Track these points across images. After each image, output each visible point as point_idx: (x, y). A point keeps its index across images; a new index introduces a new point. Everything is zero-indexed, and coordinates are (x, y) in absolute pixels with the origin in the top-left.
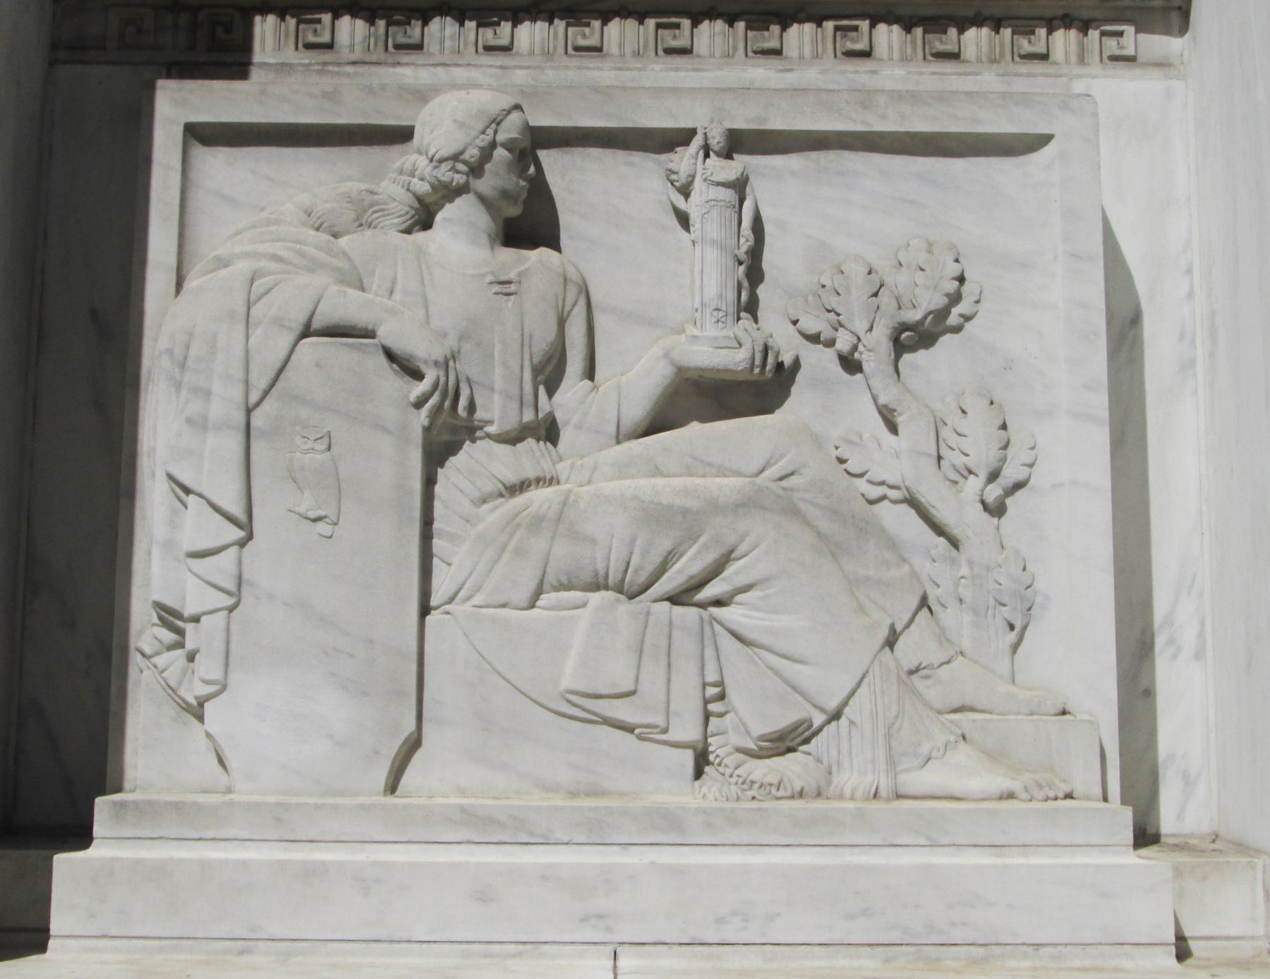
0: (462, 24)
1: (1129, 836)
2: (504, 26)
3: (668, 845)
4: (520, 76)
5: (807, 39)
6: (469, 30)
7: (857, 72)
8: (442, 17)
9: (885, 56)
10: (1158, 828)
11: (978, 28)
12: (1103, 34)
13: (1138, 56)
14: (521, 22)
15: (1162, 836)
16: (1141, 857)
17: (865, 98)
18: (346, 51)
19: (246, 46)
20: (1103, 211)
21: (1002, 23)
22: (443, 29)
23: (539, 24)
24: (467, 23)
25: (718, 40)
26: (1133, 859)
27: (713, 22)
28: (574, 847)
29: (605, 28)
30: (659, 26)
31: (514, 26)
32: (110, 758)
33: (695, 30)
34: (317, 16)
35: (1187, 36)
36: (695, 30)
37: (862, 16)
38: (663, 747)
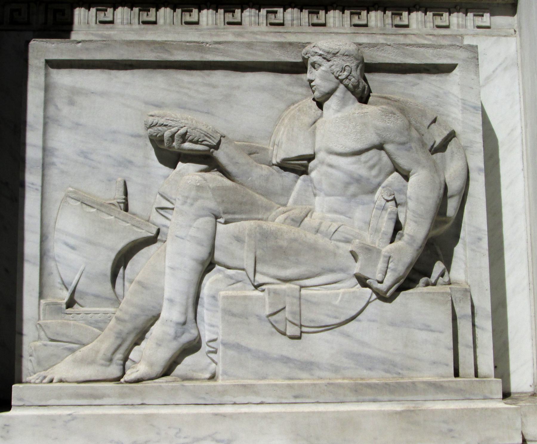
0: (343, 13)
1: (501, 396)
2: (152, 10)
3: (159, 405)
4: (363, 39)
5: (168, 15)
6: (220, 14)
7: (107, 31)
8: (250, 9)
9: (332, 25)
10: (510, 391)
11: (457, 13)
12: (434, 15)
13: (285, 23)
14: (117, 8)
15: (512, 393)
16: (506, 403)
17: (107, 43)
18: (456, 28)
19: (70, 23)
20: (481, 101)
21: (428, 9)
22: (303, 14)
23: (211, 11)
24: (219, 10)
25: (210, 16)
26: (501, 405)
27: (251, 9)
28: (237, 405)
29: (327, 15)
30: (268, 12)
31: (157, 10)
32: (16, 367)
33: (285, 12)
34: (401, 12)
35: (516, 16)
36: (285, 12)
37: (279, 6)
38: (209, 359)
